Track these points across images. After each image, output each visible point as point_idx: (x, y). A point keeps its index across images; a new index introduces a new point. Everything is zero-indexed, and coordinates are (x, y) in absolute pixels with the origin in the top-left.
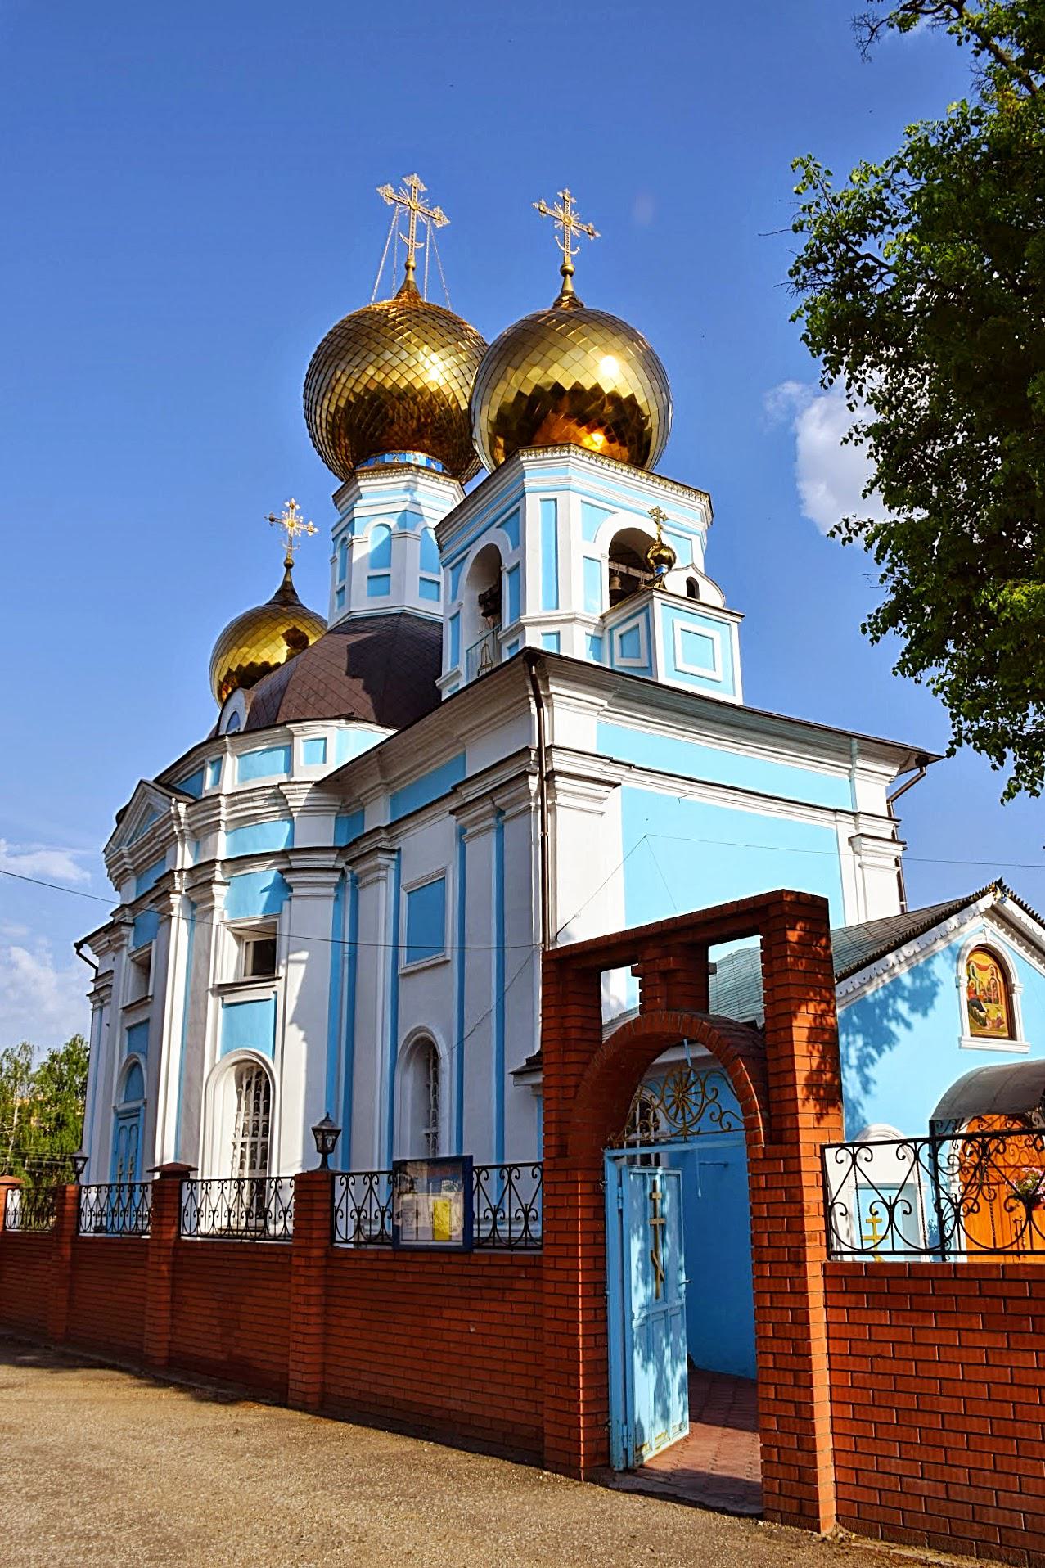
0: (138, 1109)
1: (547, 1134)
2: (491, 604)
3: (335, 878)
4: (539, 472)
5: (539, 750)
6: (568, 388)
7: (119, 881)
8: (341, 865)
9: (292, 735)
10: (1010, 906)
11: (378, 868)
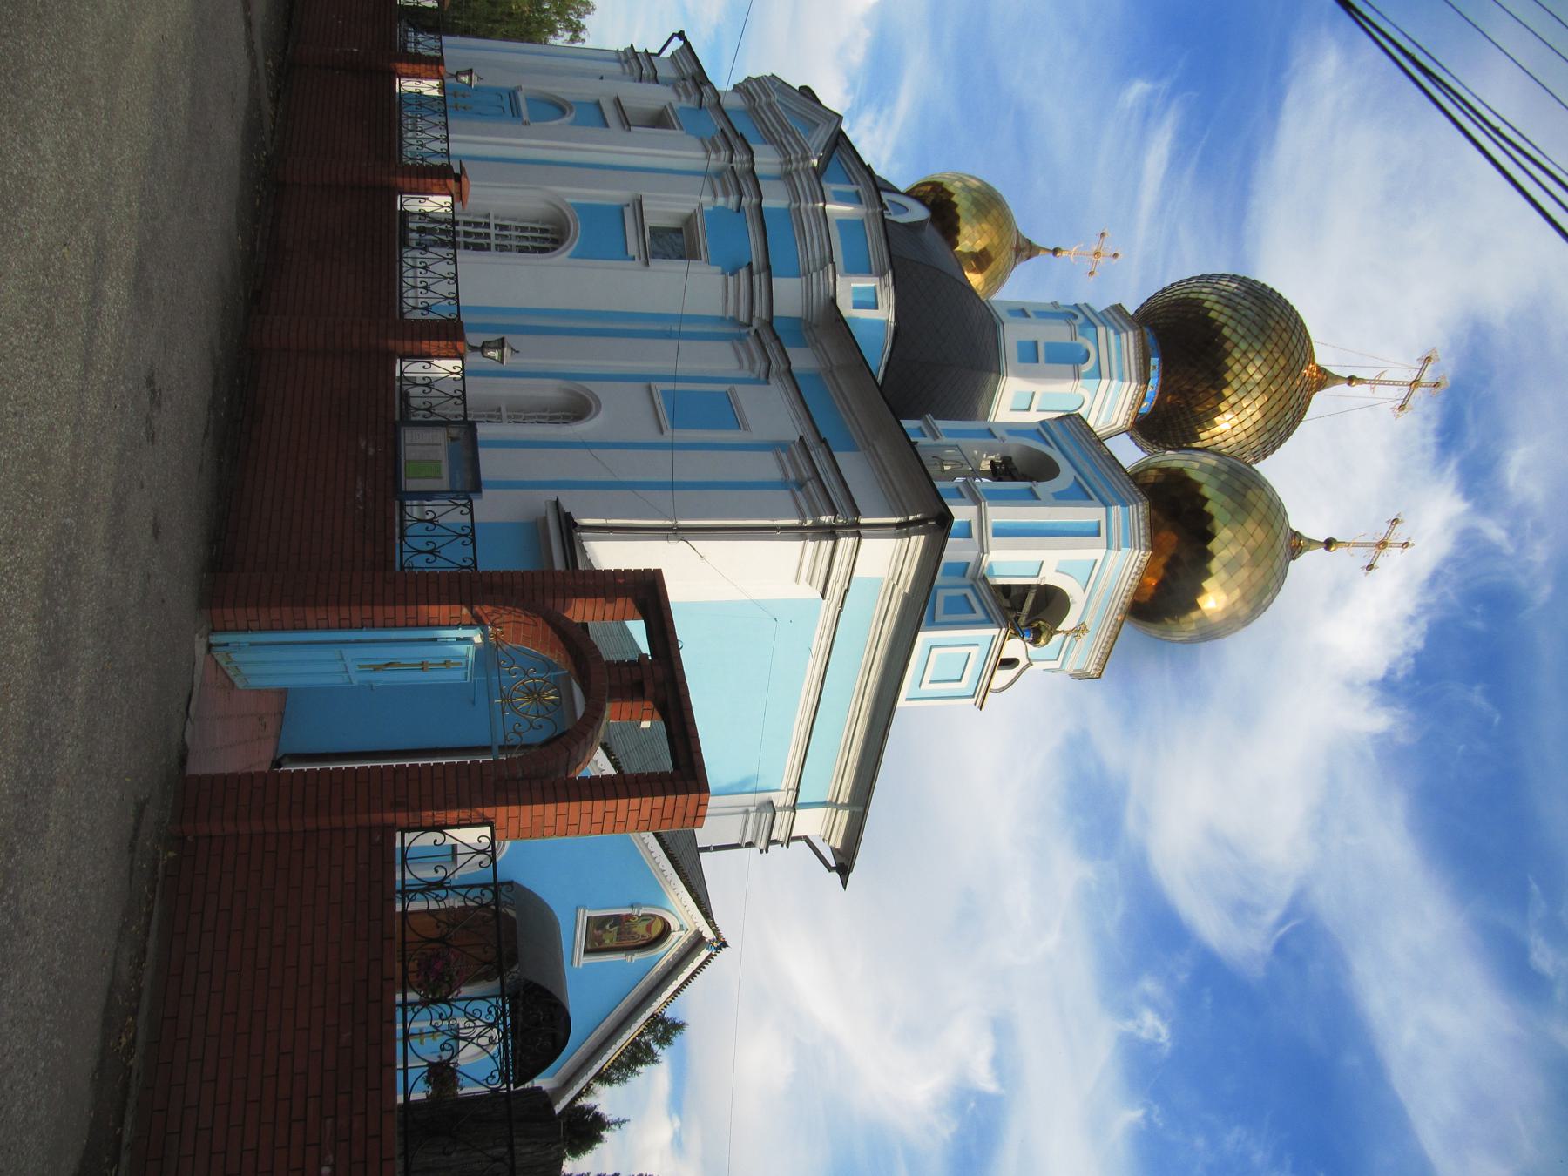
0: (519, 115)
1: (502, 575)
2: (1004, 470)
3: (743, 317)
4: (1128, 517)
5: (858, 525)
6: (1209, 547)
7: (741, 89)
8: (756, 324)
9: (881, 274)
10: (705, 953)
11: (752, 361)
